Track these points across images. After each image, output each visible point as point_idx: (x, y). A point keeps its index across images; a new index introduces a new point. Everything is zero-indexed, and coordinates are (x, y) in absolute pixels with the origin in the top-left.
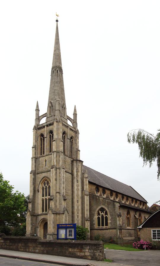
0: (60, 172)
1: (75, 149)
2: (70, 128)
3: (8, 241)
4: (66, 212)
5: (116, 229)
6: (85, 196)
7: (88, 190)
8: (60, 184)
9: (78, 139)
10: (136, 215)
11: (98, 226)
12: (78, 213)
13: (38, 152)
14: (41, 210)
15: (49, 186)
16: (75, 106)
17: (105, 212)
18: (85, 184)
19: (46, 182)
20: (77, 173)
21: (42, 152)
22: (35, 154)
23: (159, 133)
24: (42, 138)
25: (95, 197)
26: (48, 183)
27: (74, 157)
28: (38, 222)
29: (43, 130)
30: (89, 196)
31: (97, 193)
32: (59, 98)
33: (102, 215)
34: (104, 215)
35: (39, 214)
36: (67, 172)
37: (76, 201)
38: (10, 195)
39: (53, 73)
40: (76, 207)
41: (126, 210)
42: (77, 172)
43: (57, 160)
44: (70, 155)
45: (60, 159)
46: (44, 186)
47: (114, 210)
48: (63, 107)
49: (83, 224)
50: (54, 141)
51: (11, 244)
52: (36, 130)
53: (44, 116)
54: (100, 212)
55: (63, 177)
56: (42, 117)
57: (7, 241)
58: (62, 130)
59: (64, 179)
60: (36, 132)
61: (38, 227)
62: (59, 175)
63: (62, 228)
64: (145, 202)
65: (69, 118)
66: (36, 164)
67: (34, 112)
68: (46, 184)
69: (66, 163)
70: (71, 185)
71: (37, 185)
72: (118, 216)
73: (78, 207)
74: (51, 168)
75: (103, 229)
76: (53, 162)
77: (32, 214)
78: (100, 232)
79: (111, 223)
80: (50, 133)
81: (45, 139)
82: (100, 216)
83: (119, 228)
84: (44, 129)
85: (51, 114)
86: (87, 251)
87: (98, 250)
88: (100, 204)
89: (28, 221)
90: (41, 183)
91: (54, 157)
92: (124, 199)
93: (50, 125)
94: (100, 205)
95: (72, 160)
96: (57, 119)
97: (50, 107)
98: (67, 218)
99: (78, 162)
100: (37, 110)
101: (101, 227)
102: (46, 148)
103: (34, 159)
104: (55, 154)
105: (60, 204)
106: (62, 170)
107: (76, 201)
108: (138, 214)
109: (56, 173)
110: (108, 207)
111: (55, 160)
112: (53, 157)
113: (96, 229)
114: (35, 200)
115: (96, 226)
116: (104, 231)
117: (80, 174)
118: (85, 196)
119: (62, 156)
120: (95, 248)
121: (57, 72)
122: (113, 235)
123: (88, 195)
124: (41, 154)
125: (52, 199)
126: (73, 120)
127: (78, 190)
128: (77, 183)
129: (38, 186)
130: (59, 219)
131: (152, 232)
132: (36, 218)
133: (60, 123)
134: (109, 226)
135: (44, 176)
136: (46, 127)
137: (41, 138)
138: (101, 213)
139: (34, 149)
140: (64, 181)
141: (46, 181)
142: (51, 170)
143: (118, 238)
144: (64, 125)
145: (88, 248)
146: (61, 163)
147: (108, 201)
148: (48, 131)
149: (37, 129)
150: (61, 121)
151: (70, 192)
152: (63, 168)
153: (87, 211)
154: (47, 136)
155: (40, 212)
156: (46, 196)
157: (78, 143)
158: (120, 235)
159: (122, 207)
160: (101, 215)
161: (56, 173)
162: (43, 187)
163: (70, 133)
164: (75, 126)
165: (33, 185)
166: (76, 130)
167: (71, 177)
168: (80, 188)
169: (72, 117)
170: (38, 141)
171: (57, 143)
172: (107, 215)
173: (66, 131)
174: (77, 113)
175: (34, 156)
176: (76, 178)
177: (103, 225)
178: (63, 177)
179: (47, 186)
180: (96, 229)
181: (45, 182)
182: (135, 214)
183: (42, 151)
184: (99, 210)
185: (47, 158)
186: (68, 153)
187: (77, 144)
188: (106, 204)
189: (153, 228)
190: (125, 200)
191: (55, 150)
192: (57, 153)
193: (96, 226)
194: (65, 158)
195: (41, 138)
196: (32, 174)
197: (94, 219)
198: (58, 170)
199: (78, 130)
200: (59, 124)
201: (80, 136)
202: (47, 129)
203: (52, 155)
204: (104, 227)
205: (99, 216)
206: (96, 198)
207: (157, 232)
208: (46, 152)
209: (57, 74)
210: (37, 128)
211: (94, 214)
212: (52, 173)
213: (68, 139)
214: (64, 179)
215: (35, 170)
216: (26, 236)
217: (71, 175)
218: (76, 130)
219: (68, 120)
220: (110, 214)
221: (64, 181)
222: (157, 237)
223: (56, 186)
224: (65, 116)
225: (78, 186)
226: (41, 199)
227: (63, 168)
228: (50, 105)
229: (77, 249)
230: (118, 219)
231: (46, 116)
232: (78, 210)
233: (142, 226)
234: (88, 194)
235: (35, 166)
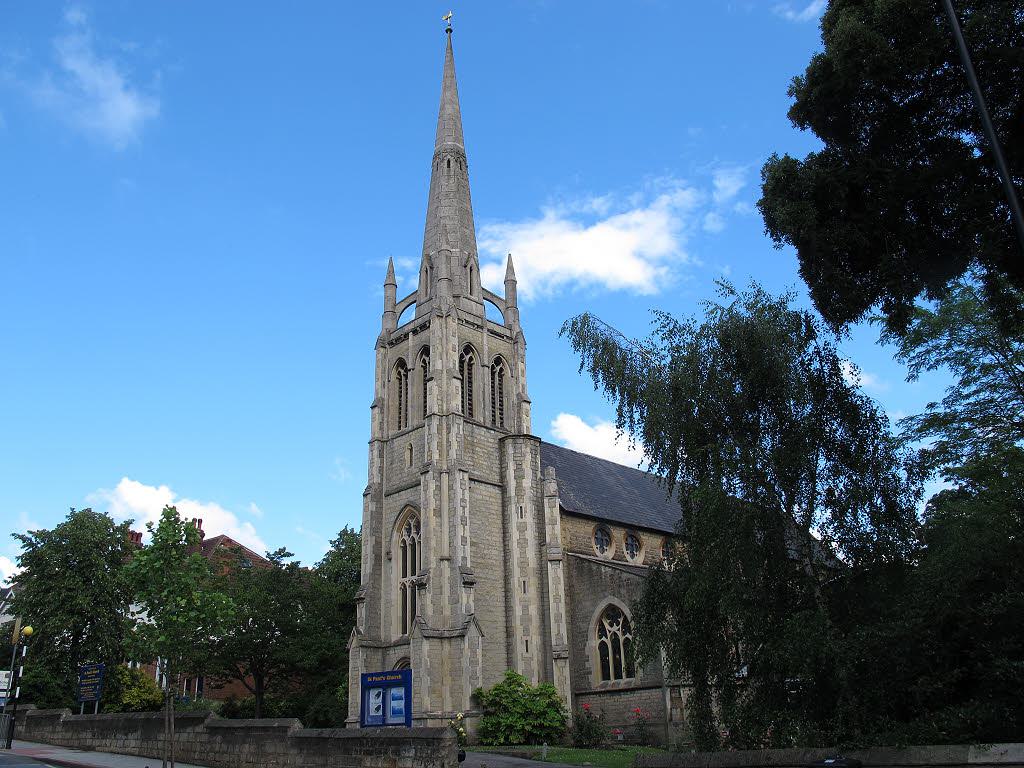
4: (472, 631)
5: (661, 687)
8: (453, 528)
11: (604, 679)
12: (526, 631)
14: (400, 630)
17: (621, 620)
22: (381, 429)
24: (402, 371)
31: (603, 551)
34: (619, 634)
36: (482, 482)
37: (516, 586)
38: (310, 572)
40: (518, 611)
42: (519, 477)
43: (440, 445)
44: (494, 421)
45: (453, 438)
48: (465, 266)
49: (547, 675)
50: (432, 379)
53: (412, 300)
55: (463, 500)
63: (374, 685)
65: (490, 297)
66: (382, 462)
70: (501, 526)
73: (525, 608)
75: (619, 692)
78: (609, 700)
80: (422, 354)
87: (437, 758)
98: (479, 651)
100: (391, 285)
101: (613, 680)
106: (459, 476)
107: (516, 586)
109: (439, 488)
112: (427, 433)
113: (596, 693)
114: (379, 589)
115: (596, 681)
116: (625, 697)
117: (527, 483)
119: (458, 428)
121: (449, 166)
123: (559, 561)
126: (506, 302)
127: (523, 543)
128: (520, 520)
133: (450, 320)
135: (403, 503)
140: (467, 514)
142: (422, 478)
144: (467, 322)
145: (412, 753)
146: (453, 454)
151: (495, 552)
152: (460, 470)
158: (674, 711)
160: (609, 635)
161: (439, 488)
162: (404, 541)
163: (487, 346)
164: (511, 321)
168: (531, 534)
176: (514, 500)
177: (618, 676)
178: (463, 500)
180: (596, 693)
181: (409, 525)
183: (403, 414)
184: (601, 616)
185: (413, 438)
186: (482, 414)
188: (623, 591)
193: (596, 681)
198: (445, 477)
200: (446, 323)
205: (604, 639)
210: (391, 340)
215: (381, 484)
216: (347, 727)
217: (497, 491)
221: (467, 514)
223: (439, 534)
224: (475, 292)
225: (522, 529)
226: (399, 586)
227: (460, 470)
228: (425, 263)
231: (415, 302)
232: (526, 618)
234: (559, 556)
235: (381, 469)
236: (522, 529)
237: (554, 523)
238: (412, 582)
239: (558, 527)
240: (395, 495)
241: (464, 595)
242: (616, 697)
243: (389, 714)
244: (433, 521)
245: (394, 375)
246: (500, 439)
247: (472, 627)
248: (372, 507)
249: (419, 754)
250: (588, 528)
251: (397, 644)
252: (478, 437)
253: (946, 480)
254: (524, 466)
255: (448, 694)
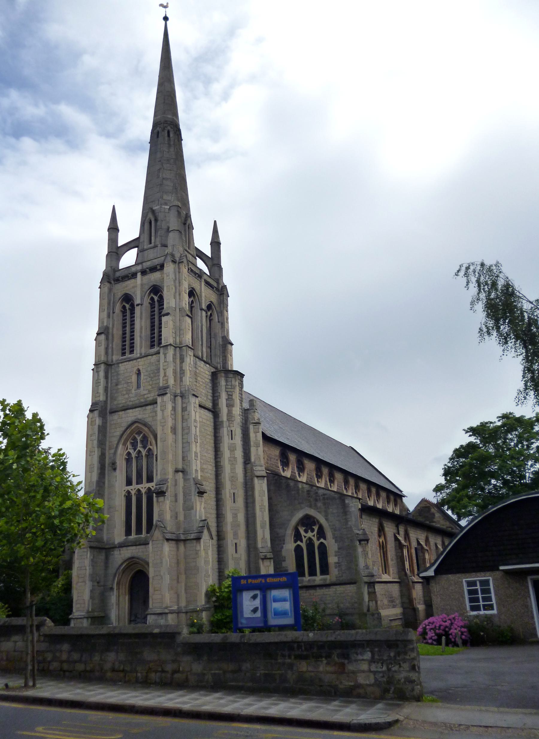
0: (184, 405)
1: (220, 340)
2: (205, 280)
3: (66, 647)
6: (256, 480)
7: (262, 462)
9: (227, 311)
10: (399, 534)
12: (236, 535)
13: (114, 347)
14: (123, 532)
15: (150, 450)
16: (215, 222)
17: (316, 528)
18: (252, 443)
19: (139, 438)
20: (228, 410)
21: (127, 347)
22: (107, 353)
23: (537, 300)
25: (284, 481)
26: (145, 441)
27: (218, 361)
28: (112, 570)
29: (130, 283)
30: (265, 478)
32: (178, 200)
33: (310, 539)
34: (315, 539)
35: (116, 542)
39: (156, 136)
40: (229, 518)
41: (374, 520)
42: (230, 405)
43: (175, 372)
46: (131, 451)
47: (347, 521)
50: (168, 314)
51: (76, 656)
52: (110, 283)
53: (129, 246)
54: (302, 530)
56: (125, 248)
57: (58, 647)
58: (187, 287)
59: (198, 429)
60: (110, 290)
61: (112, 589)
62: (183, 416)
64: (399, 493)
65: (201, 255)
66: (107, 383)
67: (105, 235)
68: (139, 445)
69: (199, 379)
70: (213, 445)
71: (110, 449)
72: (360, 541)
73: (235, 516)
74: (159, 395)
75: (314, 587)
76: (165, 375)
77: (93, 544)
79: (338, 565)
80: (150, 292)
81: (137, 310)
82: (302, 541)
83: (366, 579)
84: (133, 281)
85: (153, 241)
86: (365, 666)
87: (404, 661)
88: (299, 503)
89: (80, 568)
90: (122, 441)
91: (165, 362)
92: (350, 487)
93: (153, 269)
94: (302, 508)
95: (213, 370)
96: (173, 255)
97: (150, 223)
99: (231, 375)
100: (113, 229)
102: (141, 337)
103: (102, 367)
104: (171, 351)
105: (189, 508)
108: (402, 529)
109: (174, 409)
110: (326, 512)
111: (170, 372)
116: (320, 592)
118: (256, 480)
120: (392, 654)
121: (169, 135)
122: (348, 605)
123: (264, 477)
124: (124, 354)
125: (161, 493)
126: (212, 258)
127: (233, 460)
128: (231, 441)
129: (112, 451)
130: (186, 557)
131: (466, 588)
132: (107, 558)
134: (334, 573)
135: (133, 419)
136: (139, 275)
137: (124, 307)
138: (306, 532)
139: (103, 337)
140: (198, 434)
141: (139, 433)
143: (365, 615)
145: (368, 655)
147: (324, 495)
148: (147, 287)
149: (112, 282)
150: (185, 260)
152: (194, 395)
153: (263, 527)
154: (142, 299)
155: (119, 536)
156: (139, 481)
157: (228, 323)
159: (367, 510)
160: (304, 540)
162: (129, 454)
164: (217, 276)
165: (98, 447)
166: (220, 286)
167: (212, 420)
168: (239, 453)
169: (207, 251)
170: (115, 314)
171: (174, 321)
172: (325, 539)
173: (197, 288)
174: (222, 239)
175: (103, 358)
176: (226, 424)
179: (141, 450)
181: (135, 439)
182: (395, 531)
183: (127, 343)
185: (142, 364)
187: (223, 323)
188: (319, 504)
189: (468, 575)
190: (352, 489)
191: (171, 341)
192: (175, 350)
194: (196, 364)
195: (124, 307)
196: (96, 413)
197: (284, 553)
198: (179, 399)
199: (225, 287)
201: (232, 302)
202: (142, 280)
203: (162, 355)
204: (319, 579)
205: (299, 543)
206: (288, 486)
207: (481, 586)
208: (141, 348)
209: (169, 140)
211: (284, 536)
212: (163, 411)
213: (202, 309)
214: (198, 429)
215: (106, 402)
217: (209, 415)
218: (220, 286)
219: (197, 258)
220: (334, 534)
221: (198, 434)
222: (481, 603)
224: (192, 247)
225: (232, 449)
226: (124, 493)
227: (194, 395)
228: (150, 216)
229: (328, 664)
230: (360, 550)
232: (235, 525)
233: (436, 571)
235: (106, 389)
236: (232, 449)
237: (258, 446)
238: (149, 489)
239: (261, 449)
240: (121, 413)
241: (198, 504)
242: (312, 592)
243: (270, 615)
244: (170, 437)
245: (118, 308)
246: (212, 373)
247: (206, 532)
248: (98, 421)
249: (376, 657)
250: (276, 452)
251: (122, 546)
252: (199, 368)
253: (470, 436)
254: (234, 397)
255: (183, 591)
